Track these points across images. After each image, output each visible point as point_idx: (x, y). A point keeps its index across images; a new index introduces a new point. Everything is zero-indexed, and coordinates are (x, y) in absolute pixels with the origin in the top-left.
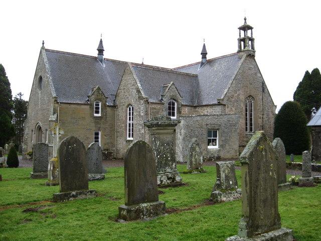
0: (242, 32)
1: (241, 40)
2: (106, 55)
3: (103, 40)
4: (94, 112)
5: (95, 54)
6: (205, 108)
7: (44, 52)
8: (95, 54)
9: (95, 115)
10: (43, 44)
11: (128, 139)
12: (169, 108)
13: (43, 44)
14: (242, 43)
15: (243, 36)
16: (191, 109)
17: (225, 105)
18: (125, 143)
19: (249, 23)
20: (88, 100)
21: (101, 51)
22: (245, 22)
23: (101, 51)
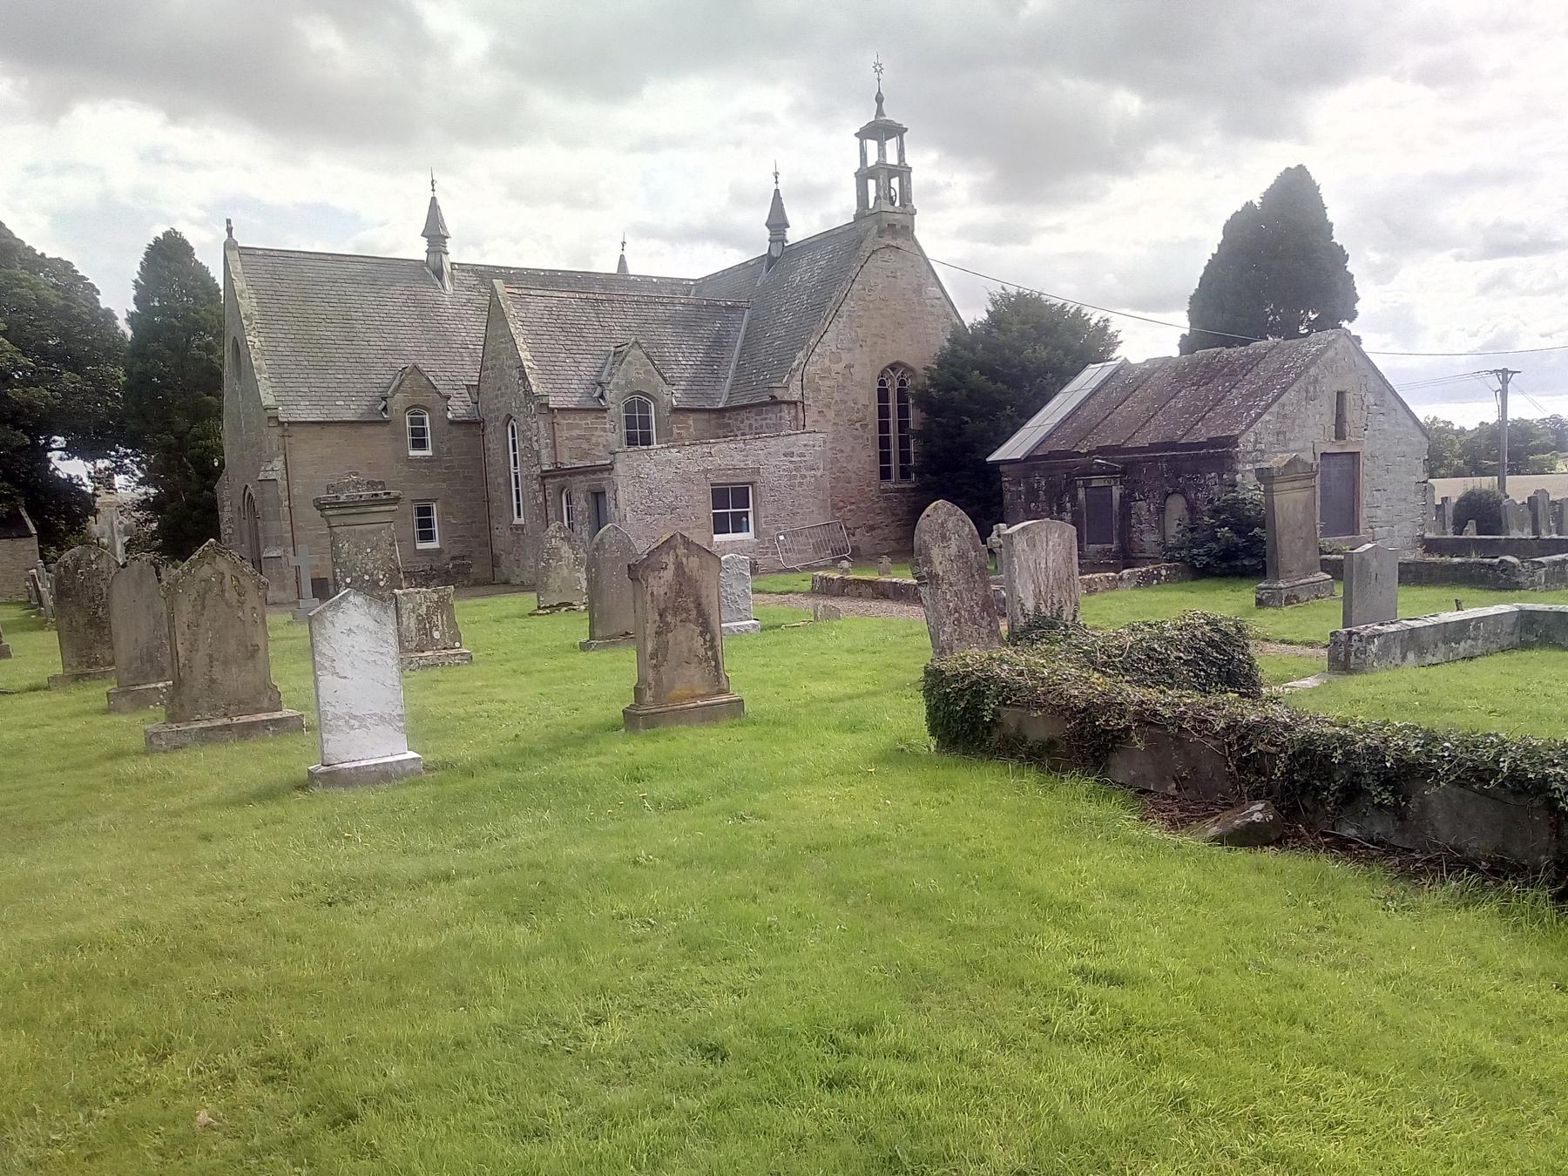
0: (872, 146)
1: (863, 176)
2: (457, 253)
3: (440, 202)
4: (409, 444)
5: (417, 250)
6: (744, 414)
7: (234, 256)
8: (417, 250)
9: (421, 546)
10: (229, 230)
11: (517, 521)
12: (630, 422)
13: (229, 230)
14: (872, 184)
15: (891, 145)
16: (709, 421)
17: (795, 403)
18: (508, 533)
19: (891, 115)
20: (385, 409)
21: (435, 233)
22: (880, 112)
23: (435, 233)
